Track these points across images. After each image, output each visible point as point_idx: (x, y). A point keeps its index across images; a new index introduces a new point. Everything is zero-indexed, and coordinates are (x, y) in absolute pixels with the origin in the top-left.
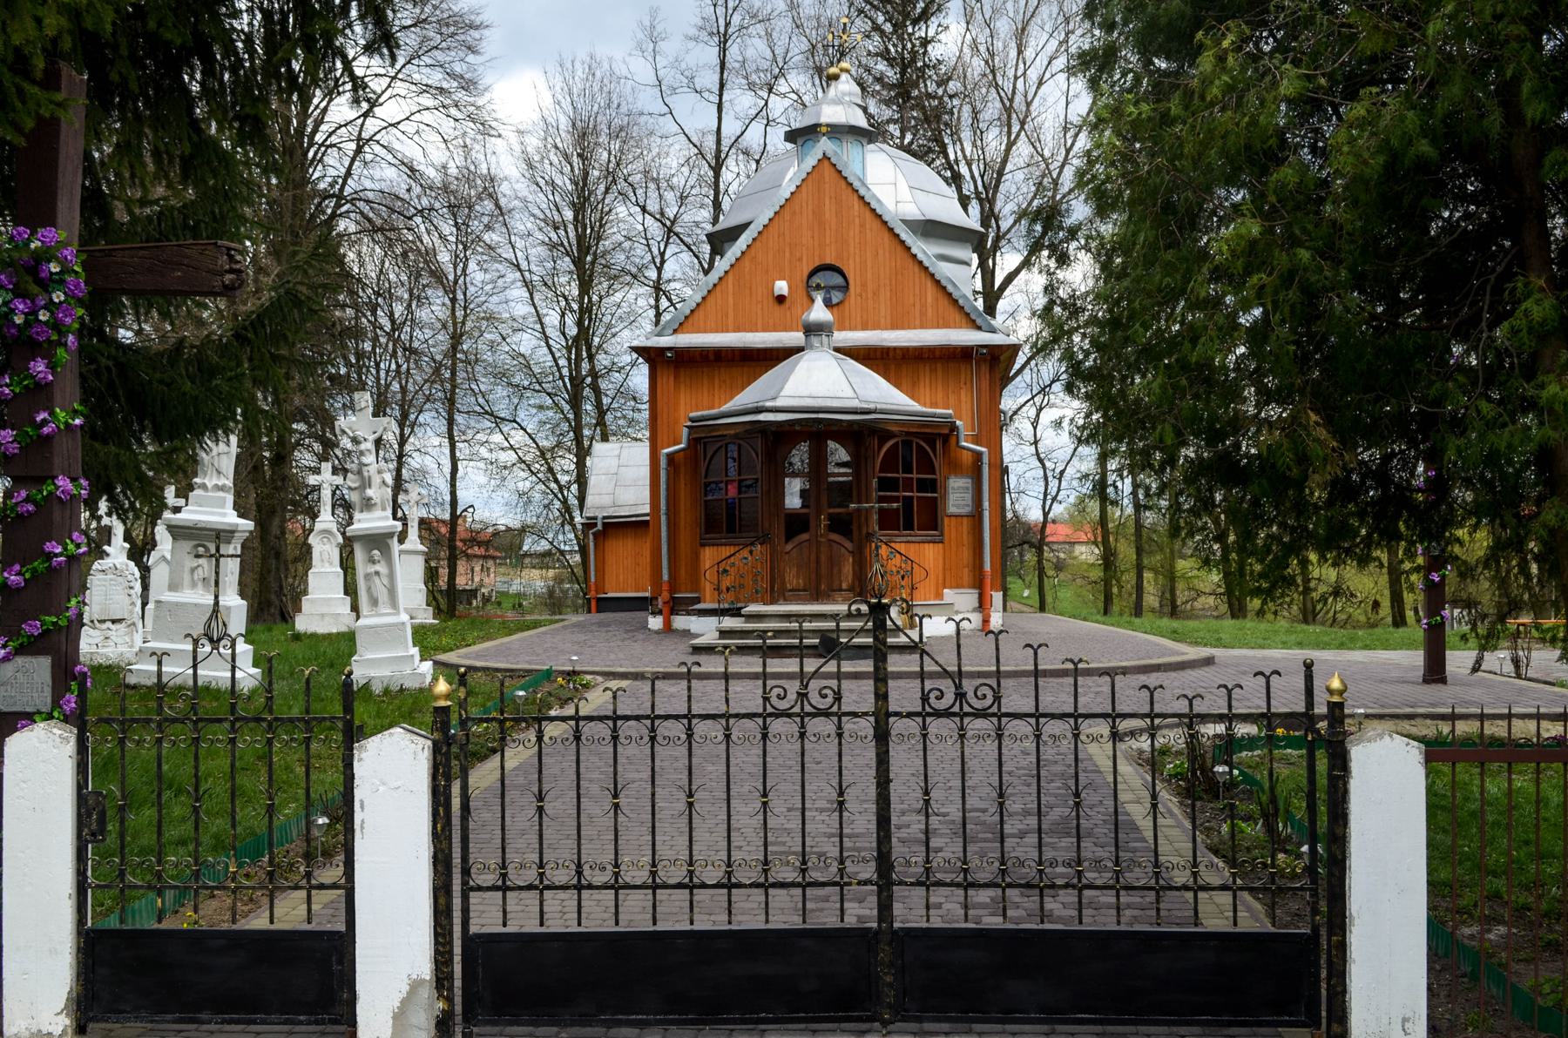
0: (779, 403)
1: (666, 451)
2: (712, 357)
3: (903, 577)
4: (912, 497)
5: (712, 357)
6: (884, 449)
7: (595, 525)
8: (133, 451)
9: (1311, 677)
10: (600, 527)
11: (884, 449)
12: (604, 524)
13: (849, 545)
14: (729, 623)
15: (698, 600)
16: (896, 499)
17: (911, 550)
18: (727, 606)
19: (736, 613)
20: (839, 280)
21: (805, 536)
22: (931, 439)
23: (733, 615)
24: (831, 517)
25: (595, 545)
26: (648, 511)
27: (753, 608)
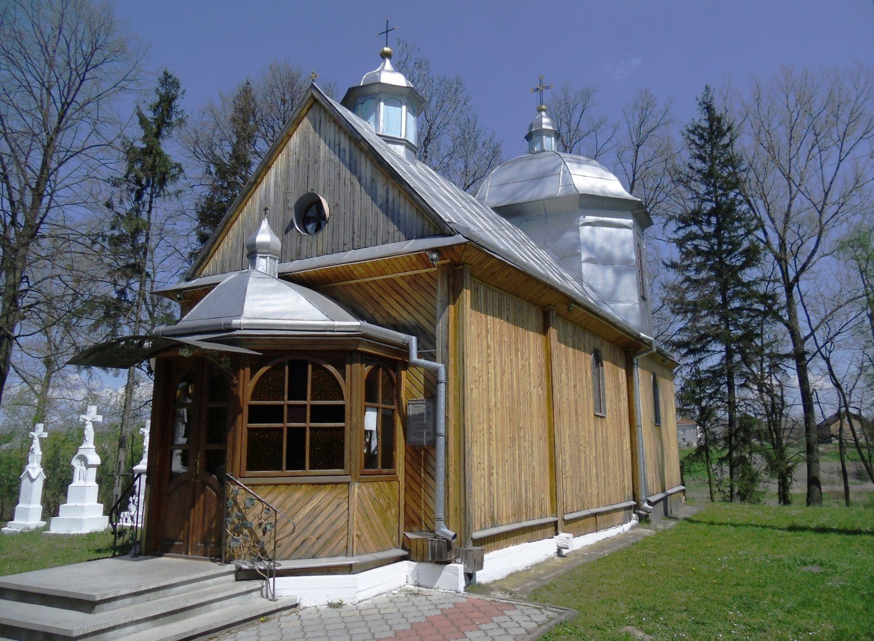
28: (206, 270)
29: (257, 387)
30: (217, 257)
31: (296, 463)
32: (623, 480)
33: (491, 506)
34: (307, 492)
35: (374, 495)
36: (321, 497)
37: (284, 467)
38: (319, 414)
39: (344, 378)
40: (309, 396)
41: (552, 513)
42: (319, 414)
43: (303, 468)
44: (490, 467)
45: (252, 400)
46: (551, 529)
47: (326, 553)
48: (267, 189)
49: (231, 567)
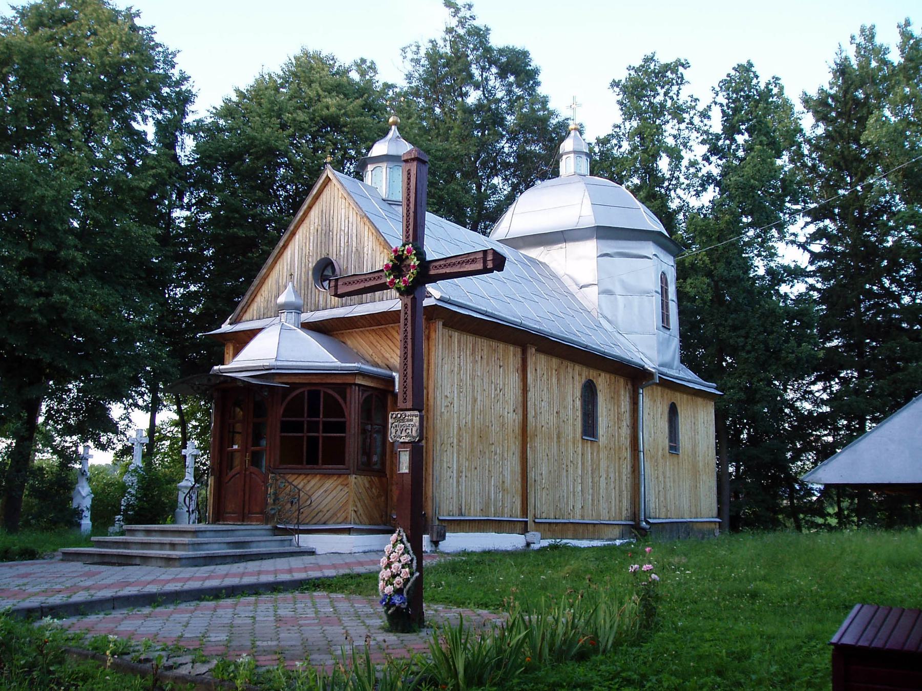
28: (247, 316)
29: (285, 411)
30: (254, 306)
31: (312, 460)
32: (620, 501)
33: (459, 498)
34: (320, 480)
35: (367, 485)
36: (330, 483)
37: (305, 463)
38: (328, 427)
39: (346, 403)
40: (302, 419)
41: (523, 515)
42: (328, 427)
43: (317, 464)
44: (460, 472)
45: (283, 417)
46: (519, 527)
47: (331, 522)
48: (293, 255)
49: (269, 526)
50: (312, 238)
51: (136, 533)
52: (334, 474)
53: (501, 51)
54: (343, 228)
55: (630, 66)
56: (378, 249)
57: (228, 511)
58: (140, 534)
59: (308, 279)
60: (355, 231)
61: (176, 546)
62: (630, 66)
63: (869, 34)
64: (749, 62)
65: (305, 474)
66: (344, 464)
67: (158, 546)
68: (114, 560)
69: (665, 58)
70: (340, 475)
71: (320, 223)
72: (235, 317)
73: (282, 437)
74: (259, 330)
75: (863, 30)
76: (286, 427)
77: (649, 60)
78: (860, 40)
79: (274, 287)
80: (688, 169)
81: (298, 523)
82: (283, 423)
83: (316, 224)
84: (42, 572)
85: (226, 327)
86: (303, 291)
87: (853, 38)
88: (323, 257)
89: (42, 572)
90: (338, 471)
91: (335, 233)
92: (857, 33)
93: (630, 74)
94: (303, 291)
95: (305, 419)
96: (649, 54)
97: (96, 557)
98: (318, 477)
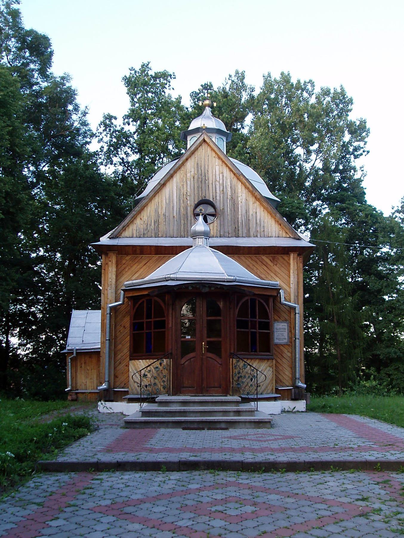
0: (179, 276)
1: (110, 305)
2: (138, 251)
3: (252, 380)
4: (256, 332)
5: (138, 251)
6: (240, 304)
7: (72, 353)
8: (13, 454)
9: (267, 470)
10: (75, 355)
11: (240, 304)
12: (77, 353)
13: (220, 361)
14: (145, 406)
15: (127, 393)
16: (161, 403)
17: (255, 364)
18: (145, 396)
19: (152, 400)
20: (211, 210)
21: (192, 355)
22: (266, 298)
23: (149, 402)
24: (208, 343)
25: (71, 367)
26: (100, 346)
27: (161, 398)
28: (127, 233)
50: (189, 182)
51: (171, 404)
52: (265, 359)
53: (31, 32)
54: (218, 179)
55: (132, 68)
56: (251, 200)
57: (185, 385)
58: (175, 405)
59: (187, 213)
60: (229, 184)
61: (241, 413)
62: (132, 68)
63: (241, 77)
64: (210, 83)
65: (250, 359)
66: (269, 352)
67: (221, 414)
68: (196, 426)
69: (155, 69)
70: (268, 359)
71: (196, 172)
72: (115, 233)
73: (238, 331)
74: (182, 248)
75: (237, 73)
76: (241, 324)
77: (145, 67)
78: (235, 79)
79: (153, 214)
80: (99, 136)
81: (248, 394)
82: (238, 321)
83: (192, 173)
84: (350, 444)
85: (104, 240)
86: (182, 222)
87: (230, 76)
88: (201, 199)
89: (350, 444)
90: (268, 357)
91: (211, 182)
92: (233, 74)
93: (131, 74)
94: (182, 222)
95: (249, 319)
96: (146, 62)
97: (196, 424)
98: (257, 361)
